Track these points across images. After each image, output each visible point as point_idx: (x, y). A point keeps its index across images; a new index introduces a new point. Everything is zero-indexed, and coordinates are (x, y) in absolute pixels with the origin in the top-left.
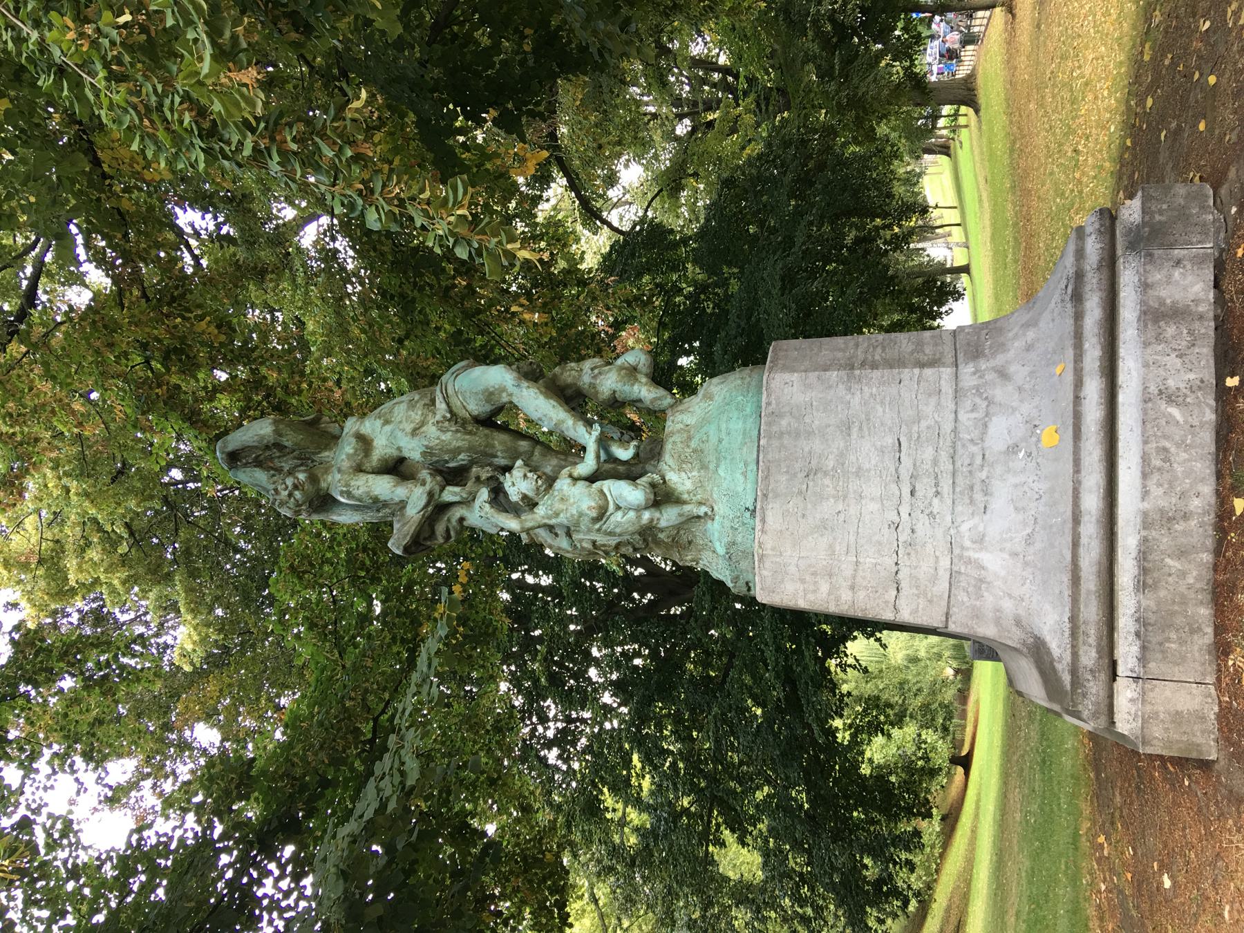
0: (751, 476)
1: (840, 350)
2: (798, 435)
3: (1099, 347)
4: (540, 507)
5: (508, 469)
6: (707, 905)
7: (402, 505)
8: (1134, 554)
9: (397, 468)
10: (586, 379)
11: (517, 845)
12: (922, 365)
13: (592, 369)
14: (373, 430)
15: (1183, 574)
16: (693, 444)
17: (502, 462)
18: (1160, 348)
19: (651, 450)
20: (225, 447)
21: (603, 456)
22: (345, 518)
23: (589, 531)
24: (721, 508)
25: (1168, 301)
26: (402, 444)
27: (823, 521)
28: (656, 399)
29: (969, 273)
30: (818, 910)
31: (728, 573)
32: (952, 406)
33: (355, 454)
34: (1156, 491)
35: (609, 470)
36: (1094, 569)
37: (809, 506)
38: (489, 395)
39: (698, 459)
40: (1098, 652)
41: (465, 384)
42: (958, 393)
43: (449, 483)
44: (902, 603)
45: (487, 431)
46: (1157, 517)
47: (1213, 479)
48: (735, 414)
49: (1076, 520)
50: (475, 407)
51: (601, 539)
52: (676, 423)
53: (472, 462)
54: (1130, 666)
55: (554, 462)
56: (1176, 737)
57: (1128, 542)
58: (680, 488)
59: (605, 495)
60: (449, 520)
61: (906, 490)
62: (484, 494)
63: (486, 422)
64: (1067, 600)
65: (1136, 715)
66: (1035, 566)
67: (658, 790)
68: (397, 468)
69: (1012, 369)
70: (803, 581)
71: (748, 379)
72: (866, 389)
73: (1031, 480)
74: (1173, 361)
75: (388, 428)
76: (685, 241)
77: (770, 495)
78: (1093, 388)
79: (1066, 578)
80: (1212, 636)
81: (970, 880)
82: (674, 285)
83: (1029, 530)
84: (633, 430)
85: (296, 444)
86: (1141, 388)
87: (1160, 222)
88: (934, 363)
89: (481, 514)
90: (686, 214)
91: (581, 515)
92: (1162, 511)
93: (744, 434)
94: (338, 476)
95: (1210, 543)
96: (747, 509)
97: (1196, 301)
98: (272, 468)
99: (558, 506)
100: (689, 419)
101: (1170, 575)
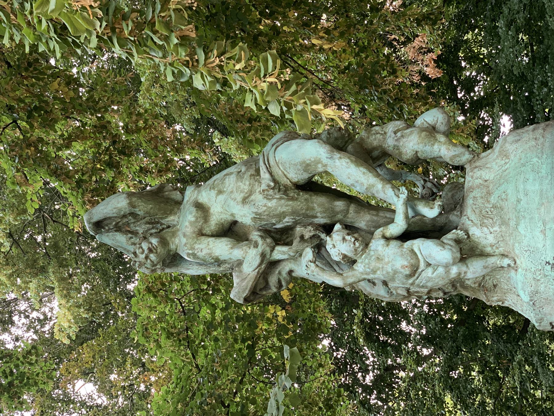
4: (359, 265)
5: (328, 229)
7: (240, 263)
9: (231, 231)
10: (390, 142)
13: (395, 133)
17: (321, 220)
21: (411, 213)
22: (195, 271)
24: (523, 262)
26: (234, 211)
28: (455, 156)
33: (196, 221)
38: (306, 166)
45: (306, 196)
48: (531, 177)
50: (296, 175)
52: (472, 179)
53: (296, 223)
58: (483, 242)
59: (415, 254)
60: (280, 273)
62: (309, 254)
68: (231, 231)
75: (221, 197)
85: (147, 213)
89: (306, 267)
91: (395, 272)
94: (184, 240)
96: (548, 263)
100: (486, 174)
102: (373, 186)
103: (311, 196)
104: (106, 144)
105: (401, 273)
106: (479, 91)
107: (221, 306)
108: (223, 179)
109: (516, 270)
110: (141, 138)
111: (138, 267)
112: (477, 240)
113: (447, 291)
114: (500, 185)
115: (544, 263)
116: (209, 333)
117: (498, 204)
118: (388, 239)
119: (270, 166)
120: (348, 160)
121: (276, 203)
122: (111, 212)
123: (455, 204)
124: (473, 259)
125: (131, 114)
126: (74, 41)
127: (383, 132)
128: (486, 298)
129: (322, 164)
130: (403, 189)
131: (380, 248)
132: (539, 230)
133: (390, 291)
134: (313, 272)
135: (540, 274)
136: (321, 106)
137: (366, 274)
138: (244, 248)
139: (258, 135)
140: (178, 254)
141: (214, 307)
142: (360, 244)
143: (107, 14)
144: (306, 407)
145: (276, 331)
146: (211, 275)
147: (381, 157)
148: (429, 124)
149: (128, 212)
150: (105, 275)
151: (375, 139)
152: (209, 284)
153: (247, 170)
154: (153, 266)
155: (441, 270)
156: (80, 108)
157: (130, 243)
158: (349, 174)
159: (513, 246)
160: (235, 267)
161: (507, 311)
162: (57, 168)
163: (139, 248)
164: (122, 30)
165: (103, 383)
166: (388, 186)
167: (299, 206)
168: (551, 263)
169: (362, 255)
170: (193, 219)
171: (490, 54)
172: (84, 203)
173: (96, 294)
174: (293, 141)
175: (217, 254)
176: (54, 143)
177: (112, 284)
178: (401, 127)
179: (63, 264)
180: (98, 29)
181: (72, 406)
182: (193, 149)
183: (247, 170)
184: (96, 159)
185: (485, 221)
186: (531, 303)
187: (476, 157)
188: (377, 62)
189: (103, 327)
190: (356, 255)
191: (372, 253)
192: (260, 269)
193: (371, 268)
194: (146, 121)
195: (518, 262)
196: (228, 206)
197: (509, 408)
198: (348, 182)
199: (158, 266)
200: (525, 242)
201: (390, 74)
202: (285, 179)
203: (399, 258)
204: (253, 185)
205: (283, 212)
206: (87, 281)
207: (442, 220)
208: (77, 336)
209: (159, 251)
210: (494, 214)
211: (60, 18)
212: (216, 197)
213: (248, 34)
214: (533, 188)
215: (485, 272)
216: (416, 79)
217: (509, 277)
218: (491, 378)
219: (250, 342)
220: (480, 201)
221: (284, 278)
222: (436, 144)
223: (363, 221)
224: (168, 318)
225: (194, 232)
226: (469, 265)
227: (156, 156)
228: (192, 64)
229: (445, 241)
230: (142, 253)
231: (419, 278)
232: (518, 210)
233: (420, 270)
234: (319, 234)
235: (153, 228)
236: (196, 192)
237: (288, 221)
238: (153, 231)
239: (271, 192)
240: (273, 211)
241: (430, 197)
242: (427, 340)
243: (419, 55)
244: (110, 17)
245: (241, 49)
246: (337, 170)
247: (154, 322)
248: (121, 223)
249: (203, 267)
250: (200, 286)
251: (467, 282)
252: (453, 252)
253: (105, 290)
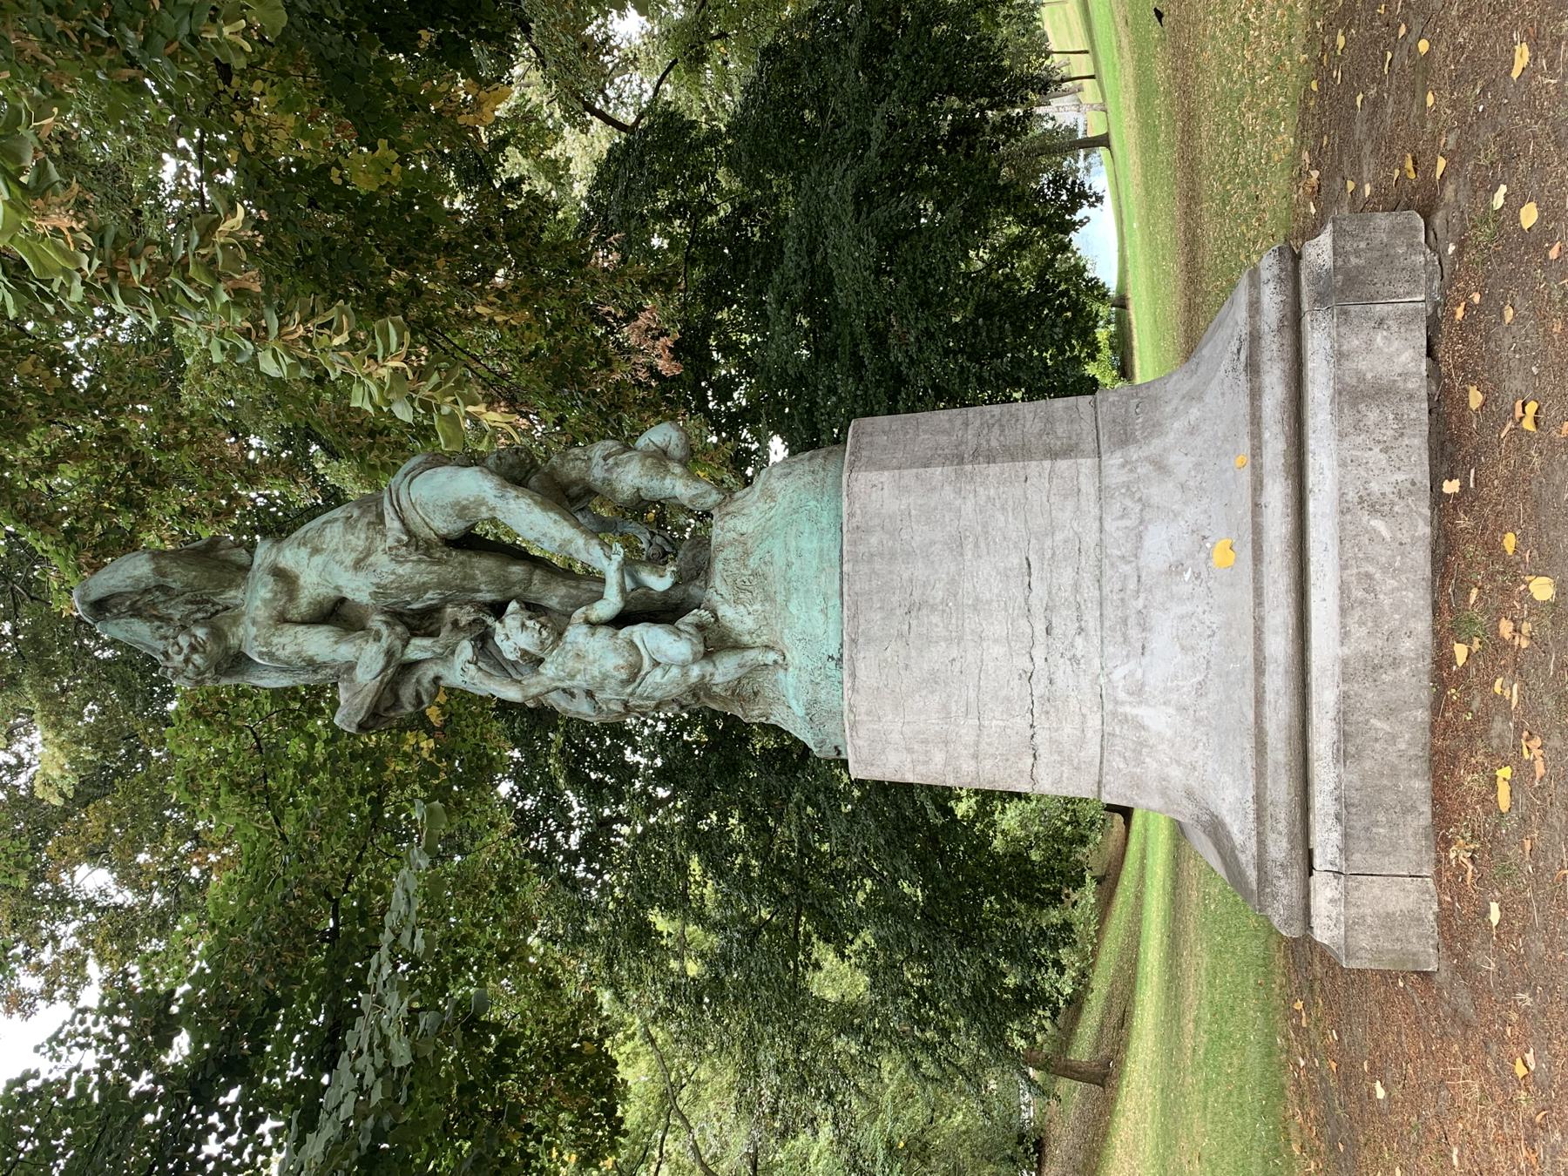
0: (833, 614)
1: (944, 432)
2: (893, 556)
3: (1282, 438)
5: (498, 610)
6: (802, 1041)
7: (351, 667)
8: (1332, 714)
9: (336, 614)
10: (598, 473)
11: (545, 1034)
12: (1054, 455)
13: (605, 459)
15: (1393, 738)
16: (753, 562)
18: (1359, 440)
22: (275, 681)
24: (795, 657)
25: (1369, 376)
27: (933, 672)
28: (696, 496)
29: (1108, 146)
30: (945, 1032)
32: (1095, 511)
33: (274, 599)
34: (1359, 632)
36: (1283, 735)
37: (914, 653)
38: (462, 510)
40: (1290, 842)
42: (1102, 492)
44: (1041, 772)
46: (1361, 667)
47: (1427, 614)
48: (807, 527)
49: (1259, 669)
50: (444, 524)
52: (722, 531)
53: (446, 601)
54: (1329, 857)
55: (562, 591)
56: (1388, 945)
57: (1325, 696)
58: (739, 627)
60: (418, 682)
61: (1040, 627)
62: (466, 649)
64: (1250, 773)
65: (1338, 920)
66: (1210, 724)
67: (725, 902)
68: (336, 614)
69: (1173, 458)
70: (910, 750)
71: (822, 474)
72: (981, 490)
73: (1200, 610)
74: (1376, 456)
75: (318, 560)
76: (714, 137)
77: (861, 640)
78: (1277, 493)
79: (1249, 745)
80: (1429, 815)
81: (1137, 960)
82: (703, 201)
83: (1199, 678)
86: (1336, 495)
87: (1357, 267)
88: (1069, 451)
89: (462, 670)
90: (716, 97)
91: (605, 676)
92: (1365, 657)
93: (821, 556)
94: (253, 631)
95: (1425, 697)
97: (1405, 375)
100: (743, 525)
101: (1376, 740)
102: (570, 541)
104: (119, 467)
106: (739, 397)
107: (324, 736)
108: (321, 531)
110: (185, 457)
116: (304, 782)
118: (592, 625)
123: (698, 571)
125: (166, 417)
126: (40, 290)
130: (617, 547)
131: (581, 639)
136: (481, 408)
139: (385, 458)
140: (244, 655)
141: (311, 739)
143: (102, 246)
144: (469, 892)
145: (419, 773)
146: (306, 686)
150: (127, 689)
152: (303, 701)
153: (362, 514)
155: (675, 671)
156: (73, 406)
161: (777, 731)
162: (29, 509)
164: (128, 275)
165: (124, 867)
166: (594, 542)
171: (754, 343)
172: (80, 568)
173: (110, 720)
176: (25, 464)
177: (139, 703)
179: (48, 671)
180: (85, 268)
181: (69, 909)
182: (276, 477)
183: (362, 514)
184: (101, 493)
188: (583, 348)
189: (123, 777)
194: (192, 431)
195: (788, 656)
197: (783, 871)
198: (531, 535)
201: (601, 366)
204: (373, 540)
206: (94, 699)
207: (678, 594)
208: (76, 791)
210: (752, 585)
211: (10, 246)
213: (369, 292)
215: (741, 672)
216: (642, 375)
218: (758, 829)
219: (374, 794)
223: (554, 596)
224: (231, 759)
225: (271, 617)
227: (210, 489)
228: (256, 333)
229: (682, 627)
230: (179, 653)
235: (199, 610)
238: (199, 615)
241: (658, 561)
242: (662, 777)
243: (647, 342)
244: (108, 251)
245: (342, 311)
247: (206, 766)
250: (287, 705)
251: (715, 689)
253: (125, 713)
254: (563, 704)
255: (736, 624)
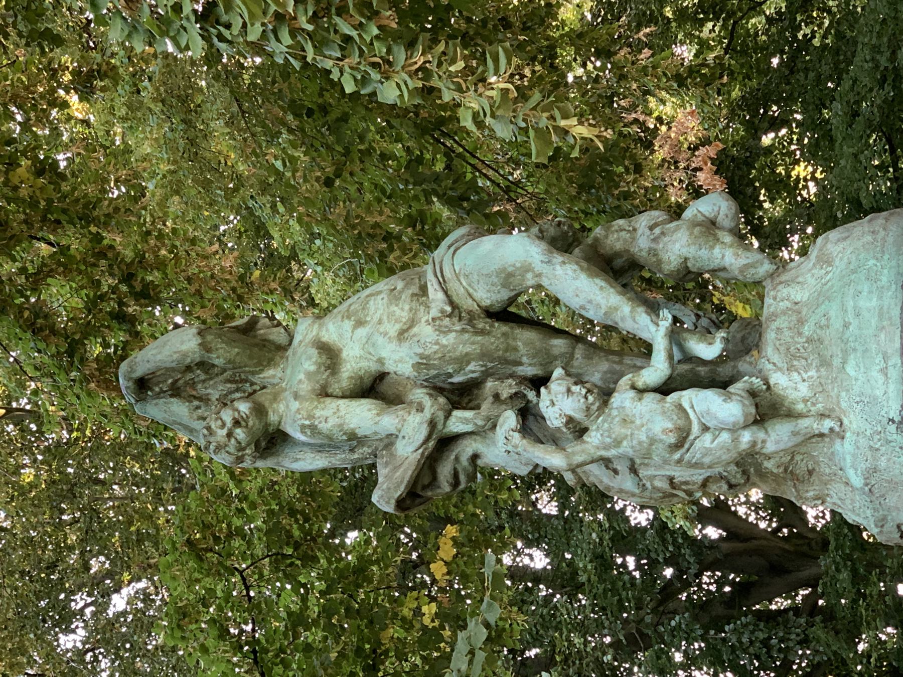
4: (593, 434)
5: (539, 382)
7: (389, 441)
9: (374, 387)
10: (642, 244)
14: (341, 336)
16: (807, 330)
17: (530, 371)
19: (743, 339)
20: (132, 371)
22: (310, 462)
23: (666, 462)
24: (854, 421)
26: (384, 354)
28: (747, 266)
31: (869, 513)
33: (318, 372)
35: (689, 375)
38: (507, 277)
39: (815, 352)
41: (469, 262)
43: (456, 405)
45: (505, 328)
48: (865, 287)
50: (488, 295)
51: (680, 475)
52: (777, 300)
53: (487, 374)
55: (605, 366)
59: (685, 411)
60: (457, 459)
62: (509, 419)
63: (502, 314)
68: (374, 387)
71: (882, 233)
75: (362, 332)
84: (722, 318)
85: (230, 362)
89: (504, 448)
91: (653, 441)
93: (881, 316)
94: (295, 405)
96: (892, 420)
98: (195, 397)
99: (619, 430)
100: (799, 294)
102: (616, 309)
103: (512, 328)
105: (661, 441)
109: (843, 438)
111: (214, 451)
112: (782, 393)
113: (733, 481)
114: (818, 306)
115: (885, 421)
117: (815, 335)
119: (444, 280)
120: (575, 267)
121: (455, 338)
122: (170, 359)
123: (747, 339)
124: (775, 420)
127: (631, 229)
128: (795, 494)
129: (533, 272)
132: (878, 367)
133: (641, 484)
134: (516, 447)
135: (879, 440)
136: (574, 121)
137: (604, 448)
138: (400, 413)
142: (595, 398)
147: (626, 271)
148: (705, 216)
149: (198, 360)
151: (618, 239)
153: (406, 286)
154: (239, 451)
157: (195, 417)
158: (577, 289)
159: (838, 396)
160: (382, 450)
163: (216, 419)
167: (492, 344)
168: (896, 420)
169: (598, 417)
170: (313, 368)
174: (484, 238)
175: (352, 426)
178: (661, 219)
183: (406, 286)
185: (795, 363)
186: (867, 489)
187: (781, 269)
190: (588, 416)
191: (615, 413)
192: (425, 449)
193: (614, 436)
195: (846, 421)
196: (374, 345)
199: (248, 451)
200: (856, 389)
202: (470, 301)
203: (659, 418)
205: (467, 354)
209: (251, 423)
212: (353, 332)
214: (868, 304)
217: (833, 453)
220: (787, 333)
221: (464, 469)
222: (718, 246)
225: (314, 390)
226: (769, 429)
231: (691, 450)
232: (845, 340)
233: (691, 437)
234: (525, 392)
236: (316, 326)
237: (473, 369)
239: (447, 321)
240: (449, 352)
246: (557, 282)
248: (181, 382)
249: (323, 455)
252: (744, 405)
254: (606, 480)
255: (789, 391)
